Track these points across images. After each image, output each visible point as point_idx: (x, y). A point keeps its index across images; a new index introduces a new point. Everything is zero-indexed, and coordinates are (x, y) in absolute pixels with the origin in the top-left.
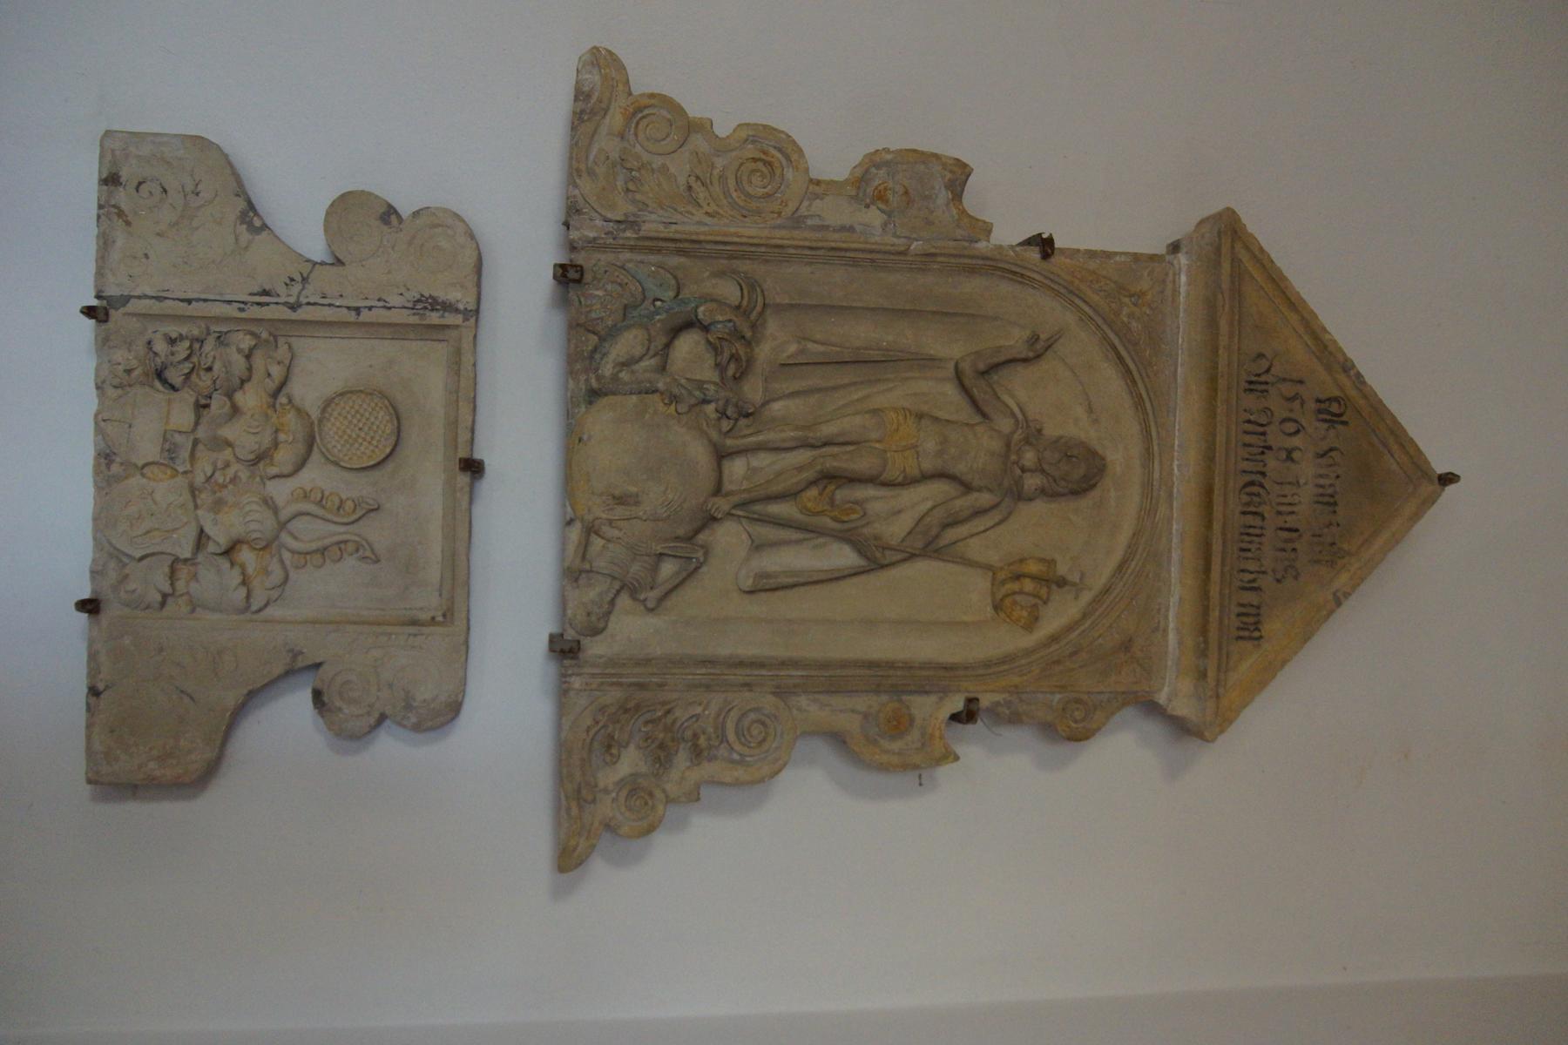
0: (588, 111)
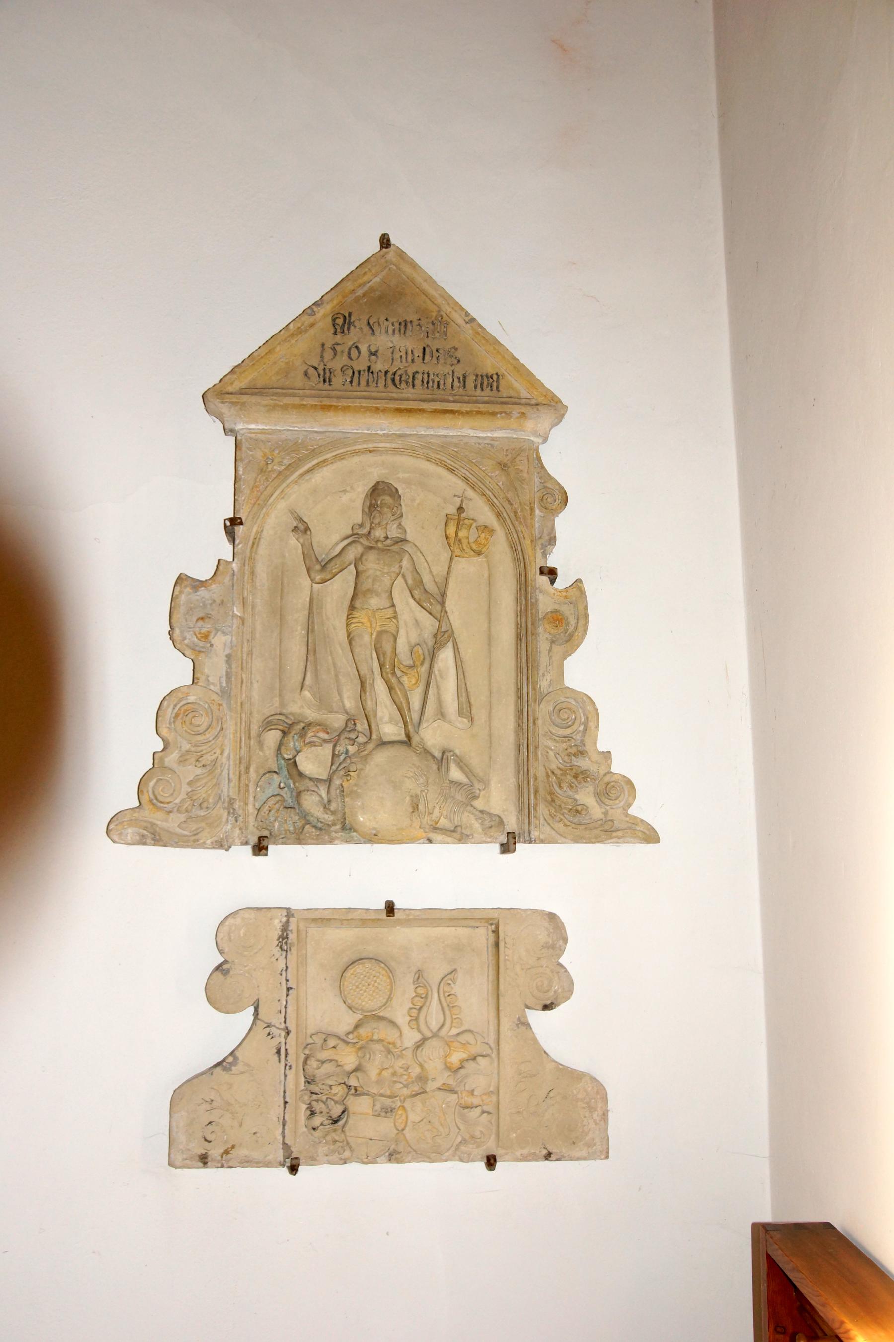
0: (153, 836)
